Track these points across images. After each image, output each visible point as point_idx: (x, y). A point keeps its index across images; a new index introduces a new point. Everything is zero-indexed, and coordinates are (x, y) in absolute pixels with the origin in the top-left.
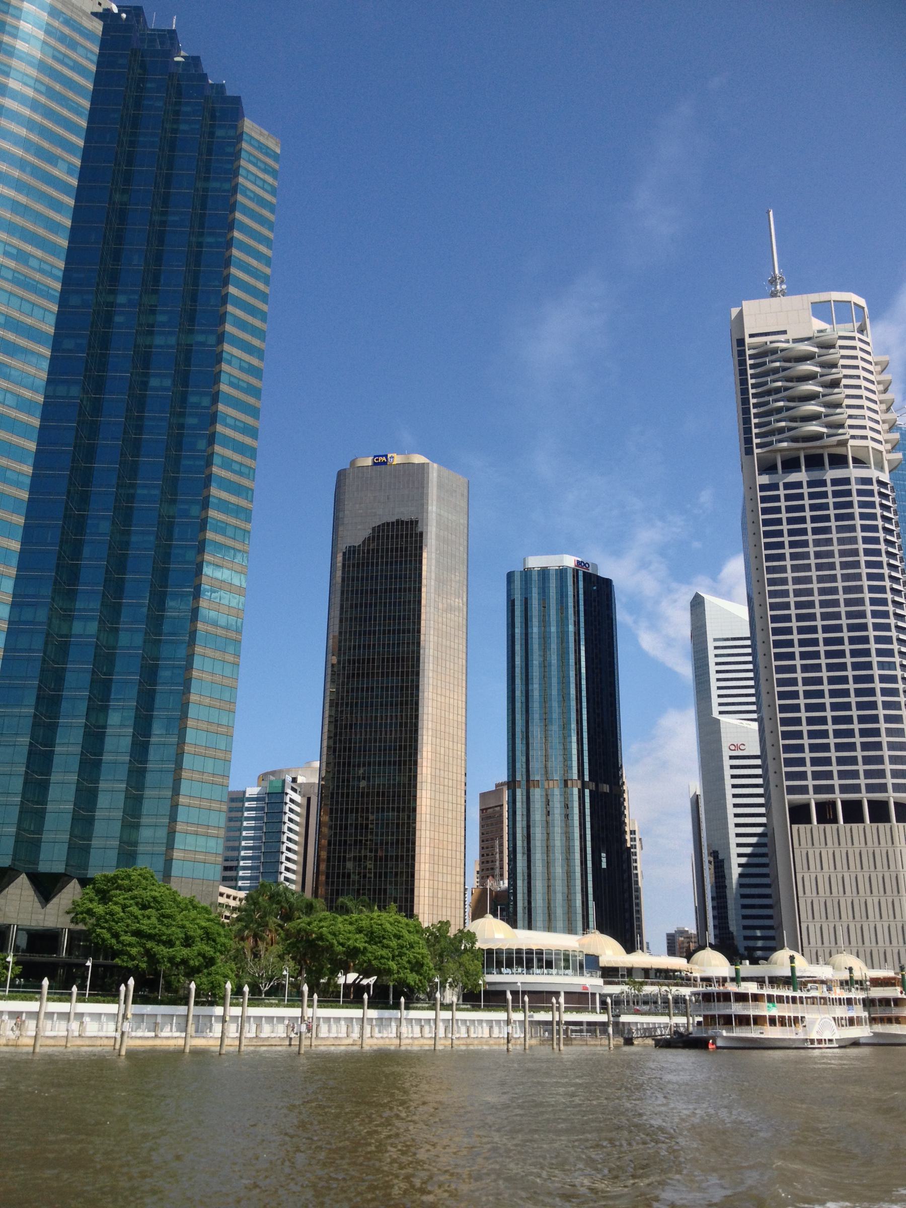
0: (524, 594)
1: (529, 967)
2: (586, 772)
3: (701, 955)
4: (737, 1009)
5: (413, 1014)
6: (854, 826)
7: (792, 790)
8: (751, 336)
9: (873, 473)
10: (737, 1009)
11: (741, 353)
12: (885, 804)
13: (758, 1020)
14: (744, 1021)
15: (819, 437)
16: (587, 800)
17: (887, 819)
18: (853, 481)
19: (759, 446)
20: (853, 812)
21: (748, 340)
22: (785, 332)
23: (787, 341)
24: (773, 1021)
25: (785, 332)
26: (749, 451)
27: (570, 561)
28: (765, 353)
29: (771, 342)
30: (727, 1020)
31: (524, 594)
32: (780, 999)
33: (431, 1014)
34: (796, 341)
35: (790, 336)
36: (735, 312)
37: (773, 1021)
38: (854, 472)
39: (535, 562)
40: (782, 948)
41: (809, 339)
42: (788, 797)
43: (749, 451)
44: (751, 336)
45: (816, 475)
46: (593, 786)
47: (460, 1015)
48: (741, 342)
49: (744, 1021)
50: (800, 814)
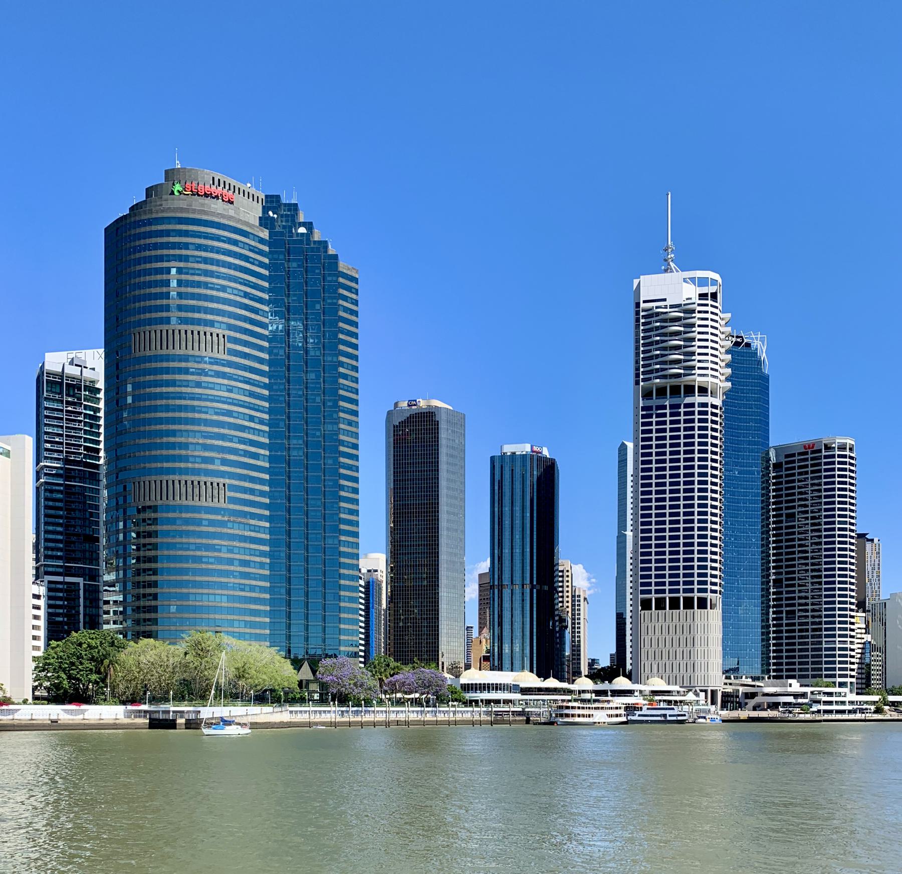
0: (501, 469)
1: (476, 689)
2: (535, 579)
3: (579, 680)
4: (567, 711)
5: (441, 709)
6: (688, 611)
7: (643, 592)
8: (645, 302)
9: (709, 400)
10: (567, 711)
11: (637, 313)
12: (705, 599)
13: (573, 716)
14: (567, 715)
15: (678, 375)
16: (535, 595)
17: (706, 608)
18: (696, 405)
19: (643, 380)
20: (674, 604)
21: (642, 305)
22: (665, 300)
23: (666, 307)
24: (579, 716)
25: (665, 300)
26: (637, 383)
27: (527, 448)
28: (651, 315)
29: (657, 307)
30: (561, 715)
31: (501, 469)
32: (583, 708)
33: (447, 709)
34: (672, 306)
35: (668, 303)
36: (636, 282)
37: (579, 716)
38: (698, 399)
39: (508, 449)
40: (619, 676)
41: (679, 306)
42: (640, 596)
43: (637, 383)
44: (645, 302)
45: (675, 401)
46: (538, 587)
47: (458, 709)
48: (638, 305)
49: (567, 715)
50: (646, 605)
